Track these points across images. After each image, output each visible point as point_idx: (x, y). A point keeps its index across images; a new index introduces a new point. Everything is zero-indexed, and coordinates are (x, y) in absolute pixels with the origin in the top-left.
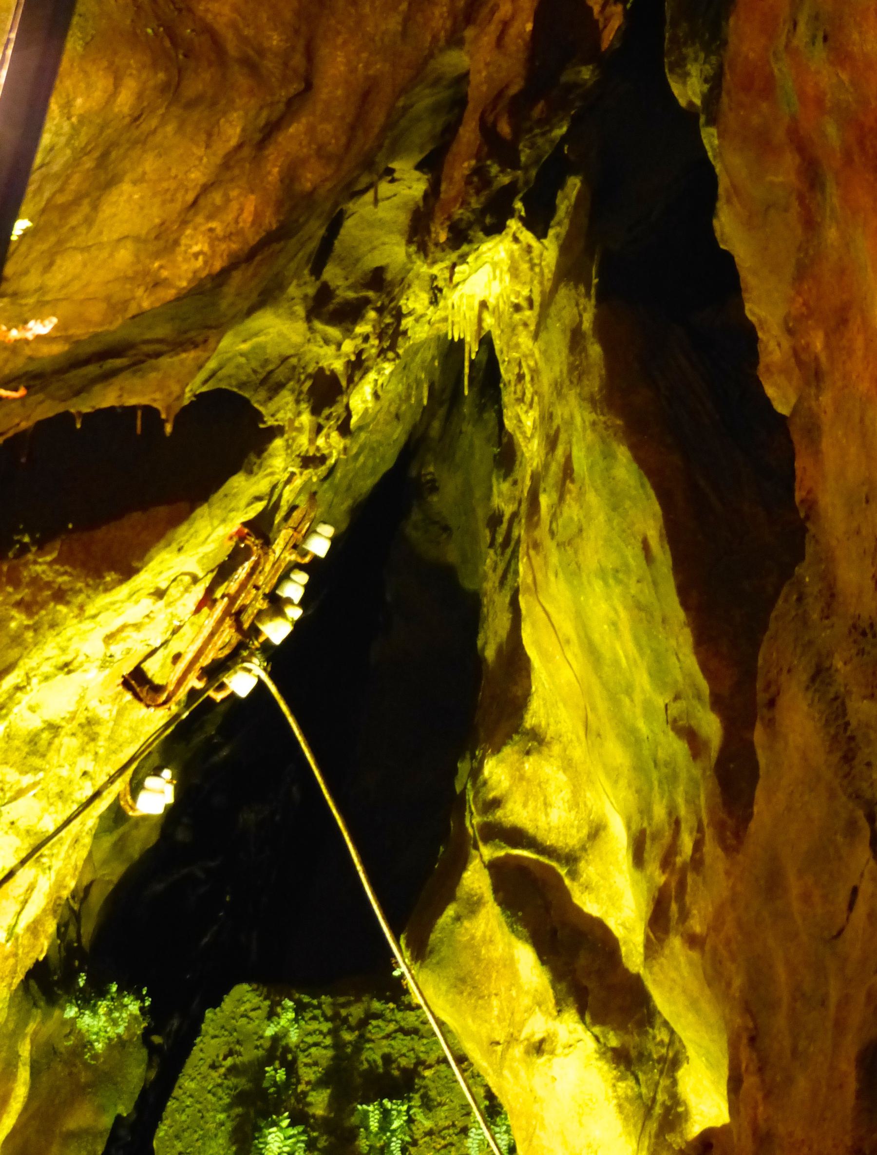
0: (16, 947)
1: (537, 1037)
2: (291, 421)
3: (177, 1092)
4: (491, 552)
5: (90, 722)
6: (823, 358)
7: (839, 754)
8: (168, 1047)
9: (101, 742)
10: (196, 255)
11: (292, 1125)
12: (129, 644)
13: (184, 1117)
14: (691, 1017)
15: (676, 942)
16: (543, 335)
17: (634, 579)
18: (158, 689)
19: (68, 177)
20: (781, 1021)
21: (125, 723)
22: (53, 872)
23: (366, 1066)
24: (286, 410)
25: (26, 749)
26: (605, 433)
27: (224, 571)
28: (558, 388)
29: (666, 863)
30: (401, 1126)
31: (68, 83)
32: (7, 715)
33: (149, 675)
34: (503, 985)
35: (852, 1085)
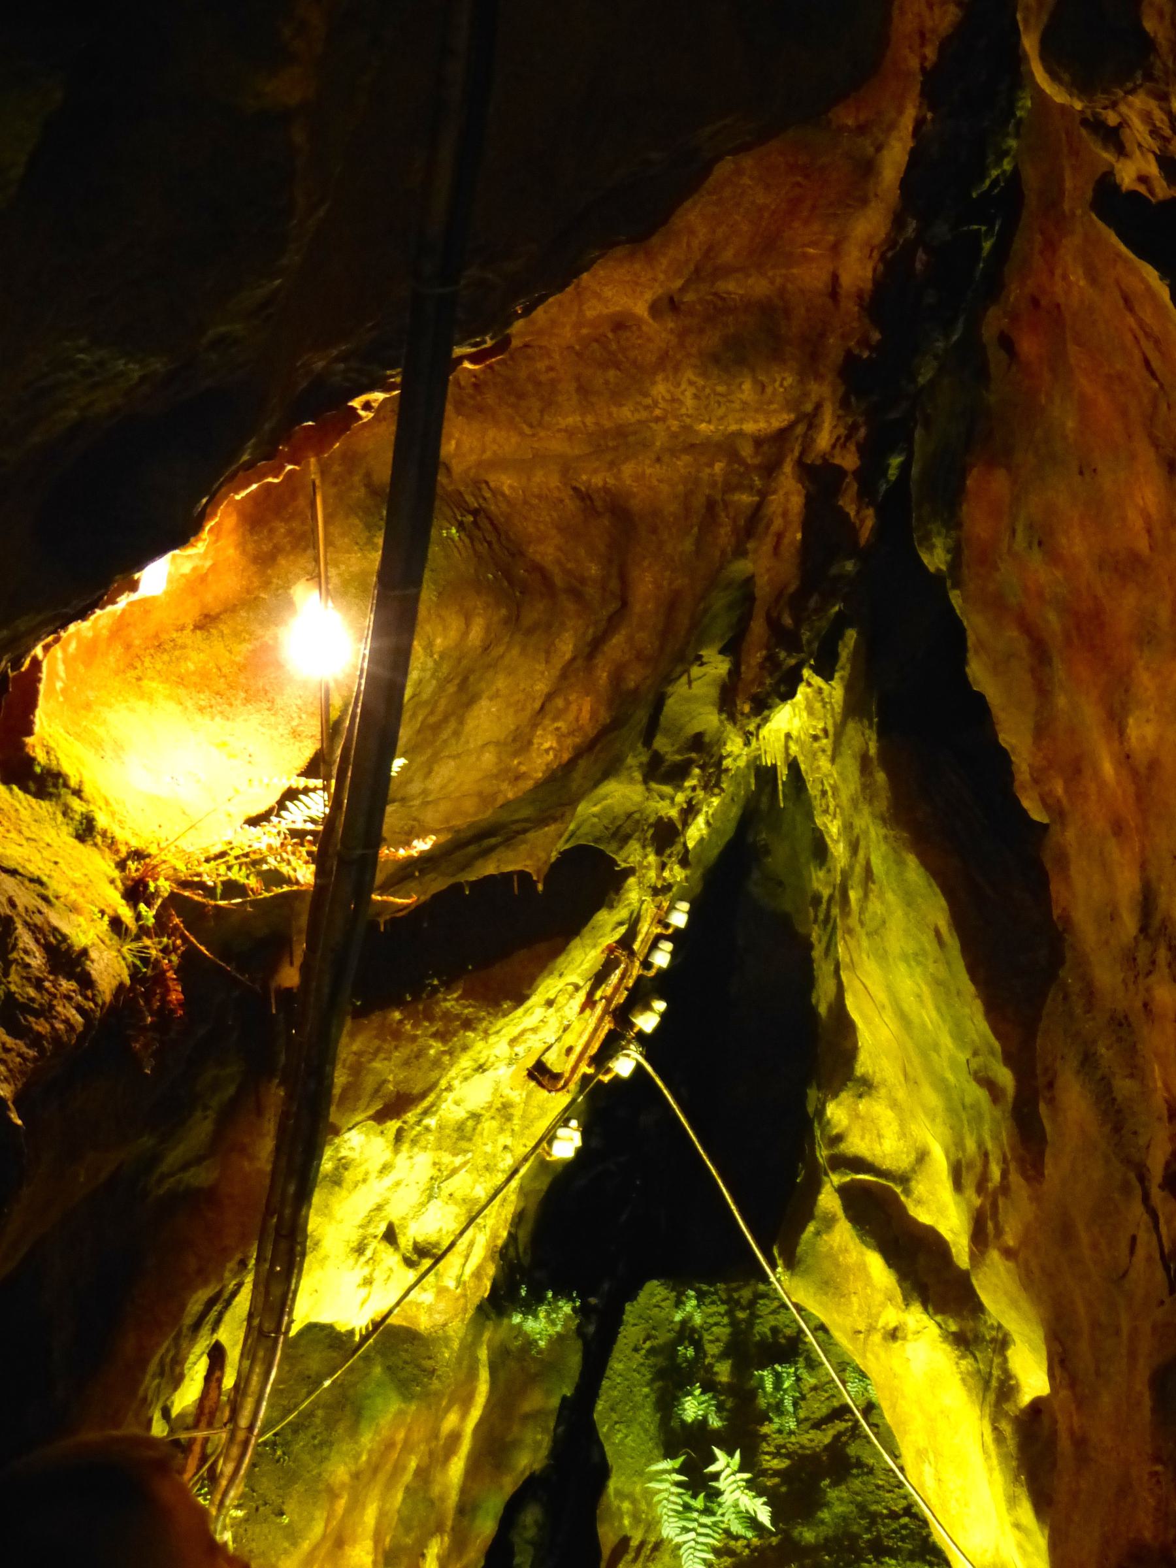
0: (465, 1289)
1: (892, 1325)
2: (640, 863)
3: (609, 1373)
4: (816, 927)
5: (506, 1106)
6: (1065, 801)
7: (1109, 1126)
8: (597, 1340)
9: (516, 1121)
10: (547, 751)
11: (702, 1393)
12: (529, 1044)
13: (616, 1393)
14: (1013, 1314)
15: (994, 1255)
16: (838, 760)
17: (931, 960)
18: (556, 1077)
19: (436, 702)
20: (1084, 1346)
21: (534, 1103)
22: (488, 1229)
23: (758, 1338)
24: (634, 854)
25: (455, 1135)
26: (895, 844)
27: (600, 978)
28: (854, 802)
29: (980, 1188)
30: (791, 1385)
31: (428, 628)
32: (437, 1111)
33: (549, 1065)
34: (859, 1286)
35: (1147, 1402)
